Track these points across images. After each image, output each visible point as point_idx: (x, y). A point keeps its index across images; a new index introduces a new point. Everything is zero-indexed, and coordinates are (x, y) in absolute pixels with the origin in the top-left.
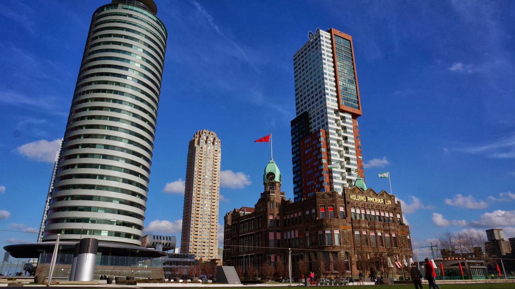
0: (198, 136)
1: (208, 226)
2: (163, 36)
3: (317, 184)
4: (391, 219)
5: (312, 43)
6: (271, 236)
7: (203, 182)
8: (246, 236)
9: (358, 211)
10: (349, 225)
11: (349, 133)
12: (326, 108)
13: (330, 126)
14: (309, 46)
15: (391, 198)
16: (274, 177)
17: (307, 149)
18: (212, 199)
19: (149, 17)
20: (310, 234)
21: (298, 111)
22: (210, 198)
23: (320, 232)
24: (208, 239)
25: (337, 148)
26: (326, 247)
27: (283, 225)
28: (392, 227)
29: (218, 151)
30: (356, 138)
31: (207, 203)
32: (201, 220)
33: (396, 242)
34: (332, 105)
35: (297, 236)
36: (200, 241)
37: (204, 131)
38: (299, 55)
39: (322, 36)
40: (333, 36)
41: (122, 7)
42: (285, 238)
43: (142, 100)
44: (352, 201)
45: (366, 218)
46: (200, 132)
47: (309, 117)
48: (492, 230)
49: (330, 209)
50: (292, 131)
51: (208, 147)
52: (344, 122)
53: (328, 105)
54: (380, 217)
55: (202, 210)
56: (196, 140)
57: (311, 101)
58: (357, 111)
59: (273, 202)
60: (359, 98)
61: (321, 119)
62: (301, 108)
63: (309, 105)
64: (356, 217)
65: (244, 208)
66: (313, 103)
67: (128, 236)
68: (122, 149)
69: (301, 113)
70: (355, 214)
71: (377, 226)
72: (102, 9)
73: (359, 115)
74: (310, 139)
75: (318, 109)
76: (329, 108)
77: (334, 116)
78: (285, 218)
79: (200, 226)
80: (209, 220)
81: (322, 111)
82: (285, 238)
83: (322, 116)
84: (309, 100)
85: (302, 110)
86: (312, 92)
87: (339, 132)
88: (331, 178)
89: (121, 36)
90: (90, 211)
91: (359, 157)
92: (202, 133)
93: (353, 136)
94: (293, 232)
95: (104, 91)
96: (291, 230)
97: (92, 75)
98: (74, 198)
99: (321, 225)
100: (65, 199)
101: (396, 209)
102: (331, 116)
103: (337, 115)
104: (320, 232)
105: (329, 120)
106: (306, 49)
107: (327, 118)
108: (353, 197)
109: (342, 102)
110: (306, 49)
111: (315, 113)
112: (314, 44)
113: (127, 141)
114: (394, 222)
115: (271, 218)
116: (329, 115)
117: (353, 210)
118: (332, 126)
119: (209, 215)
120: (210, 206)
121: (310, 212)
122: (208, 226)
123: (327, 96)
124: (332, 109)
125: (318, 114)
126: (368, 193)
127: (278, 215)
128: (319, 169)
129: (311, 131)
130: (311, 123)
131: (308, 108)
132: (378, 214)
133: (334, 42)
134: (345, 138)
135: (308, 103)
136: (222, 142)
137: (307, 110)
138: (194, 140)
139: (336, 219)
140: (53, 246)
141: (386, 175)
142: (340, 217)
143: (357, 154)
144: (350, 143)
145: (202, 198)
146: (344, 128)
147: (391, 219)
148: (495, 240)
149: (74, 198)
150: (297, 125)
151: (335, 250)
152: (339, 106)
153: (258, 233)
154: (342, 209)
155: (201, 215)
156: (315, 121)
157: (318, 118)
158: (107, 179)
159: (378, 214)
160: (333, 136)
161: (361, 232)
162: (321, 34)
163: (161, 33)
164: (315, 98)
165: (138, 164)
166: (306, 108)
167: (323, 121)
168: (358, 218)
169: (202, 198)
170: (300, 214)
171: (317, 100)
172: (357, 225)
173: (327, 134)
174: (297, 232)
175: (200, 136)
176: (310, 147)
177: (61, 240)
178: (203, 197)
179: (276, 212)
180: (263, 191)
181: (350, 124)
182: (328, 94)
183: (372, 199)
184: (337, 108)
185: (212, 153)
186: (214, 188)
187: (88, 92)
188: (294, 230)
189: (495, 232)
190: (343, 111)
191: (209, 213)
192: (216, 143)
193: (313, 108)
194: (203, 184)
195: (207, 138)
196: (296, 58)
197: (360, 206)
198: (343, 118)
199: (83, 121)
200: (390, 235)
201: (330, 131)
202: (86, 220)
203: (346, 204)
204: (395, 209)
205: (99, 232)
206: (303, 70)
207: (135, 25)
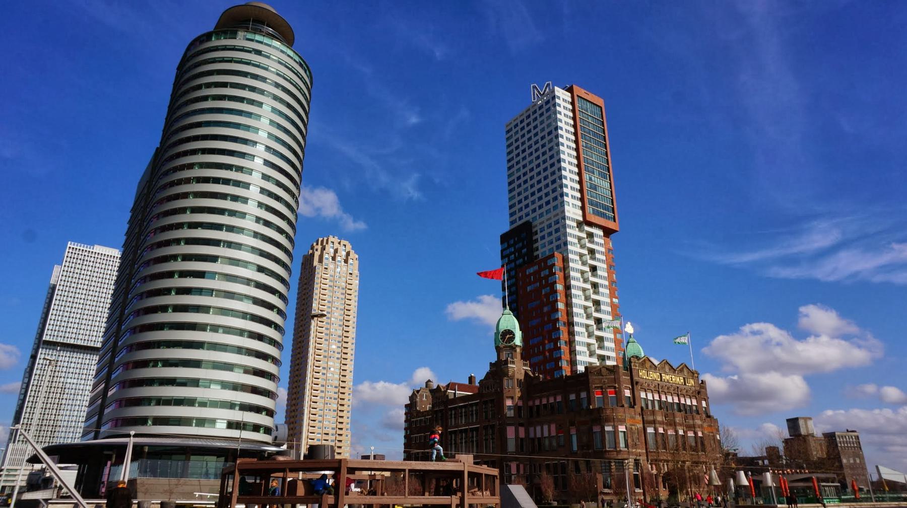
0: (319, 247)
1: (335, 406)
2: (305, 83)
3: (549, 342)
4: (694, 408)
5: (541, 107)
6: (510, 432)
7: (327, 329)
8: (461, 431)
9: (650, 397)
10: (639, 418)
11: (599, 260)
12: (564, 218)
13: (570, 247)
14: (535, 112)
15: (694, 374)
16: (513, 338)
17: (530, 283)
18: (343, 359)
19: (289, 56)
20: (578, 431)
21: (513, 218)
22: (339, 356)
23: (596, 429)
24: (333, 429)
25: (581, 284)
26: (606, 451)
27: (528, 414)
28: (698, 422)
29: (354, 276)
30: (610, 267)
31: (334, 366)
32: (323, 395)
33: (703, 444)
34: (574, 213)
35: (553, 434)
36: (320, 431)
37: (331, 239)
38: (516, 125)
39: (559, 98)
40: (576, 98)
41: (245, 36)
42: (532, 436)
43: (278, 198)
44: (641, 380)
45: (660, 408)
46: (322, 241)
47: (534, 230)
48: (797, 419)
49: (611, 393)
50: (502, 251)
51: (336, 267)
52: (592, 242)
53: (567, 214)
54: (679, 404)
55: (324, 377)
56: (317, 254)
57: (538, 204)
58: (610, 225)
59: (512, 378)
60: (615, 203)
61: (555, 236)
62: (518, 215)
63: (534, 211)
64: (647, 405)
65: (455, 384)
66: (540, 207)
67: (256, 428)
68: (248, 282)
69: (519, 223)
70: (646, 400)
71: (677, 420)
72: (208, 37)
73: (614, 231)
74: (536, 267)
75: (550, 219)
76: (569, 218)
77: (576, 232)
78: (531, 403)
79: (320, 405)
80: (336, 396)
81: (557, 222)
82: (532, 436)
83: (557, 231)
84: (533, 202)
85: (520, 218)
86: (540, 190)
87: (584, 258)
88: (571, 334)
89: (243, 87)
90: (198, 386)
91: (614, 300)
92: (327, 243)
93: (605, 266)
94: (546, 427)
95: (216, 181)
96: (542, 424)
97: (194, 152)
98: (168, 363)
99: (598, 417)
100: (151, 364)
101: (700, 391)
102: (573, 232)
103: (581, 230)
104: (596, 429)
105: (569, 239)
106: (529, 117)
107: (565, 235)
108: (642, 373)
109: (589, 209)
110: (529, 117)
111: (545, 225)
112: (544, 110)
113: (255, 268)
114: (698, 413)
115: (509, 403)
116: (568, 230)
117: (643, 395)
118: (574, 248)
119: (336, 387)
120: (338, 371)
121: (578, 396)
122: (335, 406)
123: (566, 198)
124: (573, 220)
125: (550, 226)
126: (663, 368)
127: (520, 398)
128: (552, 318)
129: (535, 254)
130: (536, 241)
131: (532, 216)
132: (676, 400)
133: (577, 109)
134: (594, 269)
135: (532, 207)
136: (360, 259)
137: (529, 218)
138: (312, 255)
139: (621, 409)
140: (124, 447)
141: (684, 340)
142: (626, 405)
143: (612, 295)
144: (601, 277)
145: (325, 357)
146: (592, 252)
147: (694, 408)
148: (800, 435)
149: (168, 363)
150: (512, 242)
151: (620, 457)
152: (584, 215)
153: (486, 428)
154: (627, 393)
155: (323, 386)
156: (543, 238)
157: (550, 234)
158: (224, 332)
159: (676, 400)
160: (575, 265)
161: (656, 429)
162: (557, 93)
163: (301, 78)
164: (545, 200)
165: (270, 306)
166: (527, 215)
167: (558, 239)
168: (650, 408)
169: (325, 357)
170: (559, 399)
171: (548, 203)
172: (651, 418)
173: (565, 260)
174: (553, 427)
175: (323, 249)
176: (534, 282)
177: (136, 436)
178: (326, 354)
179: (518, 394)
180: (494, 359)
181: (601, 245)
182: (567, 195)
183: (668, 377)
184: (581, 219)
185: (344, 279)
186: (345, 340)
187: (188, 181)
188: (549, 423)
189: (801, 422)
190: (590, 224)
191: (336, 383)
192: (350, 261)
193: (541, 215)
194: (328, 332)
195: (336, 251)
196: (511, 130)
197: (652, 387)
198: (590, 235)
199: (180, 231)
200: (695, 433)
201: (571, 256)
202: (190, 402)
203: (634, 384)
204: (699, 393)
205: (213, 422)
206: (531, 154)
207: (258, 66)
